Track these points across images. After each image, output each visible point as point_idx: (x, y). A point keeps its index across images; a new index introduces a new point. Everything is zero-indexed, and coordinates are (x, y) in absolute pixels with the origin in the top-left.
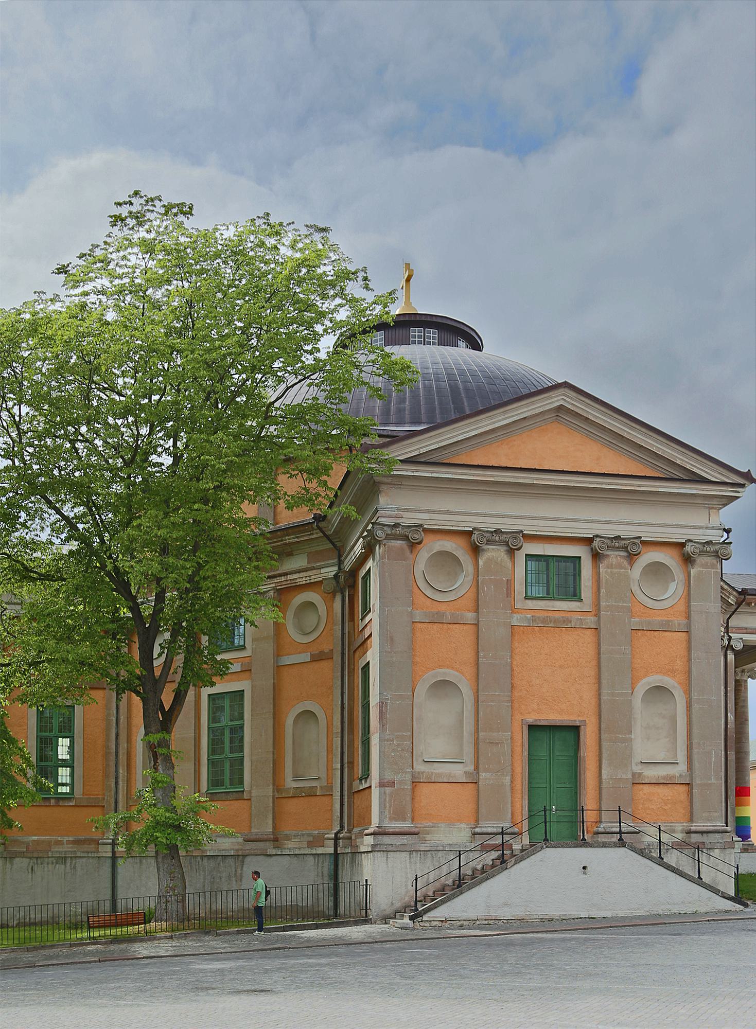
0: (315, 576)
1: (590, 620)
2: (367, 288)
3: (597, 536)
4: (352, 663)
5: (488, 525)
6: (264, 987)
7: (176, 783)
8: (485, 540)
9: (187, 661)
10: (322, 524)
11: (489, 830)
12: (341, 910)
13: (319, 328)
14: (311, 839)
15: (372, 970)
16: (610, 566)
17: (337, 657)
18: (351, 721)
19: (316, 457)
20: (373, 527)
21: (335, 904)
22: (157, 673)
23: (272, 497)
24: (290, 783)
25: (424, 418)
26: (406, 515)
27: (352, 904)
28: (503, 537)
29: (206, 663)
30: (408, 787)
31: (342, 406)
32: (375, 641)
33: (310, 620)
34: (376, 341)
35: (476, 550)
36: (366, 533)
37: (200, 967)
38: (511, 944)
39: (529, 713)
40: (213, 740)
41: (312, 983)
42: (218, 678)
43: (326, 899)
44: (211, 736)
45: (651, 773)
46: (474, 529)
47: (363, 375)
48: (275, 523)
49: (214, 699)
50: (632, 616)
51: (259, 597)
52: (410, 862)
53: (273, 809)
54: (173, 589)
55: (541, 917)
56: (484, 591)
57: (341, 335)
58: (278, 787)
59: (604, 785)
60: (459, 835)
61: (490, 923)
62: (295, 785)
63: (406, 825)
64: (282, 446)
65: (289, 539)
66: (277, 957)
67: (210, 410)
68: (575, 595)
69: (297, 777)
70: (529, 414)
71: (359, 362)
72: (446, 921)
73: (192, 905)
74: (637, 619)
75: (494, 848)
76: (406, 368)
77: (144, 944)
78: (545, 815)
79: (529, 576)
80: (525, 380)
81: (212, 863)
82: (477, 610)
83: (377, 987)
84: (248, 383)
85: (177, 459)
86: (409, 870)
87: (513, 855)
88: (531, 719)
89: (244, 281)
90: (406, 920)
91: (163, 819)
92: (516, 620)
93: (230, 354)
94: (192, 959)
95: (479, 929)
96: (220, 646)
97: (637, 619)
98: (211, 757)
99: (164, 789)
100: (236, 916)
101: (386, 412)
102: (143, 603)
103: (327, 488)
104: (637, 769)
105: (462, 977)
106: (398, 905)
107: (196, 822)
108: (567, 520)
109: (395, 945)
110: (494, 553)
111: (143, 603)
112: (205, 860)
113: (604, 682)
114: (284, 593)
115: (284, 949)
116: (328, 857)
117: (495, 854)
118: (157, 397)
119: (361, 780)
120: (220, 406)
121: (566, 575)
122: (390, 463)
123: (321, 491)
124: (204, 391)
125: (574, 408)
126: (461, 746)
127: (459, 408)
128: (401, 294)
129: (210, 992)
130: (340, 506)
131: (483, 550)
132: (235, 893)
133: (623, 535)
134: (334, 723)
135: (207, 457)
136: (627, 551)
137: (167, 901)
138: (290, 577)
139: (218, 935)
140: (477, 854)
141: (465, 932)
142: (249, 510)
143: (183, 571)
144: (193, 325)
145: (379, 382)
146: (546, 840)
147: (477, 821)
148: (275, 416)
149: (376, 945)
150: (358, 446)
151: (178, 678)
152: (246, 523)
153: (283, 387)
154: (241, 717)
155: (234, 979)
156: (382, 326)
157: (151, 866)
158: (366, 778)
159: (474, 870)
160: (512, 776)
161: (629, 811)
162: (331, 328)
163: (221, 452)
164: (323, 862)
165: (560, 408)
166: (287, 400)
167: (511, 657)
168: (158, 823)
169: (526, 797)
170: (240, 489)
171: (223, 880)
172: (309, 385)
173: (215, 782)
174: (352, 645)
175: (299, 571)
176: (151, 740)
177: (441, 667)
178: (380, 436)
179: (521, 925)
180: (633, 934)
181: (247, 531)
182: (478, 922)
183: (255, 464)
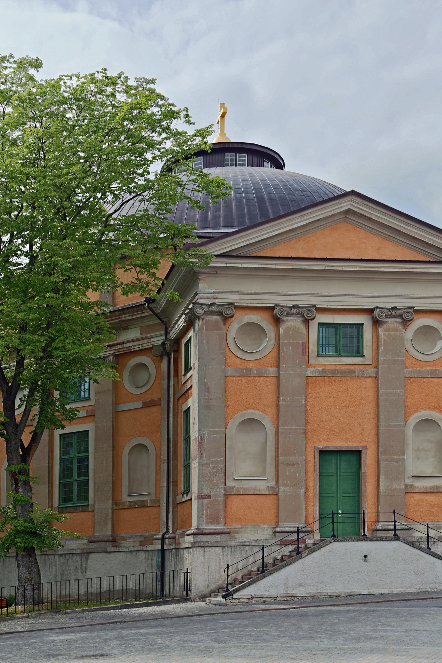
0: (146, 345)
1: (371, 371)
2: (189, 122)
3: (377, 307)
4: (176, 408)
5: (287, 302)
6: (103, 652)
7: (34, 500)
8: (285, 313)
9: (42, 411)
10: (152, 305)
11: (287, 529)
12: (167, 592)
13: (149, 156)
14: (142, 539)
15: (191, 637)
16: (388, 330)
17: (164, 404)
18: (175, 451)
19: (146, 255)
20: (193, 306)
21: (161, 589)
22: (18, 420)
23: (111, 286)
24: (126, 498)
25: (235, 222)
26: (220, 296)
27: (176, 587)
28: (300, 311)
29: (58, 411)
30: (222, 498)
31: (168, 216)
32: (195, 391)
33: (143, 376)
34: (196, 165)
35: (277, 321)
36: (187, 311)
37: (52, 638)
38: (305, 615)
39: (320, 441)
40: (63, 468)
41: (143, 648)
42: (68, 422)
43: (154, 583)
44: (62, 465)
45: (420, 484)
46: (276, 305)
47: (185, 191)
48: (114, 305)
49: (64, 438)
50: (406, 367)
51: (101, 361)
52: (223, 555)
53: (112, 517)
54: (30, 358)
55: (330, 594)
56: (284, 352)
57: (167, 161)
58: (116, 502)
59: (382, 494)
60: (263, 534)
61: (288, 599)
62: (129, 499)
63: (220, 527)
64: (119, 248)
65: (126, 317)
66: (114, 629)
67: (59, 220)
68: (358, 352)
69: (131, 494)
70: (322, 216)
71: (182, 181)
72: (252, 598)
73: (45, 591)
74: (410, 369)
75: (291, 543)
76: (220, 185)
77: (7, 624)
78: (333, 517)
79: (321, 339)
80: (320, 191)
81: (62, 560)
82: (278, 366)
83: (195, 650)
84: (91, 199)
85: (33, 259)
86: (222, 561)
87: (306, 548)
88: (321, 446)
89: (86, 122)
90: (219, 599)
91: (22, 528)
92: (309, 372)
93: (75, 179)
94: (45, 633)
95: (279, 604)
96: (69, 398)
97: (410, 369)
98: (62, 481)
99: (24, 506)
100: (81, 599)
101: (204, 218)
102: (6, 368)
103: (156, 278)
104: (408, 481)
105: (265, 641)
106: (213, 587)
107: (50, 529)
108: (353, 296)
109: (210, 617)
110: (292, 323)
111: (6, 368)
112: (57, 557)
113: (382, 417)
114: (121, 358)
115: (121, 622)
116: (156, 552)
117: (291, 548)
118: (16, 213)
119: (183, 494)
120: (68, 219)
121: (352, 337)
122: (207, 257)
123: (151, 280)
124: (55, 207)
125: (359, 210)
126: (265, 468)
127: (264, 213)
128: (217, 128)
129: (60, 658)
130: (166, 292)
131: (283, 321)
132: (81, 582)
133: (399, 306)
134: (162, 453)
135: (57, 258)
136: (402, 318)
137: (25, 590)
138: (126, 345)
139: (66, 613)
140: (277, 548)
141: (267, 606)
142: (92, 296)
143: (38, 344)
144: (45, 156)
145: (199, 196)
146: (333, 536)
147: (277, 523)
148: (114, 225)
149: (195, 618)
150: (181, 245)
151: (35, 423)
152: (90, 306)
153: (119, 202)
154: (87, 450)
155: (79, 647)
156: (201, 153)
157: (12, 563)
158: (187, 493)
159: (275, 560)
160: (306, 490)
161: (403, 513)
162: (158, 156)
163: (69, 253)
164: (152, 557)
165: (348, 211)
166: (124, 212)
167: (306, 400)
168: (18, 531)
169: (317, 504)
170: (85, 280)
171: (71, 572)
172: (141, 201)
173: (66, 498)
174: (176, 394)
175: (133, 341)
176: (13, 470)
177: (248, 409)
178: (199, 237)
179: (314, 600)
180: (405, 606)
181: (91, 312)
182: (278, 599)
183: (96, 261)
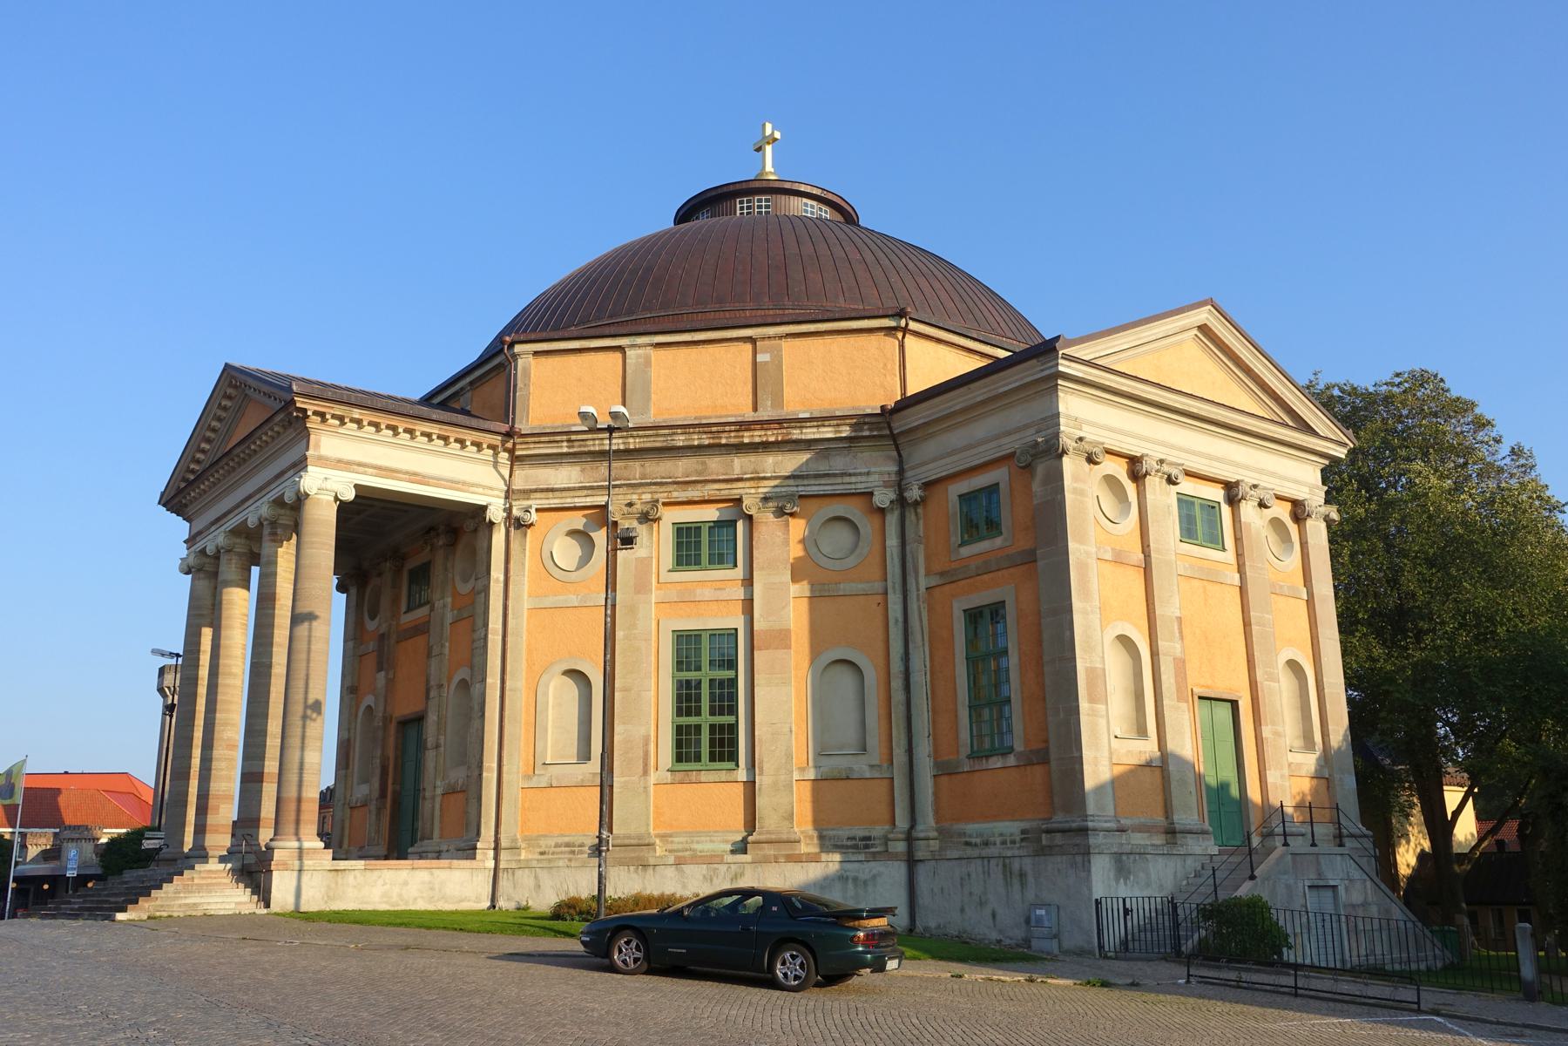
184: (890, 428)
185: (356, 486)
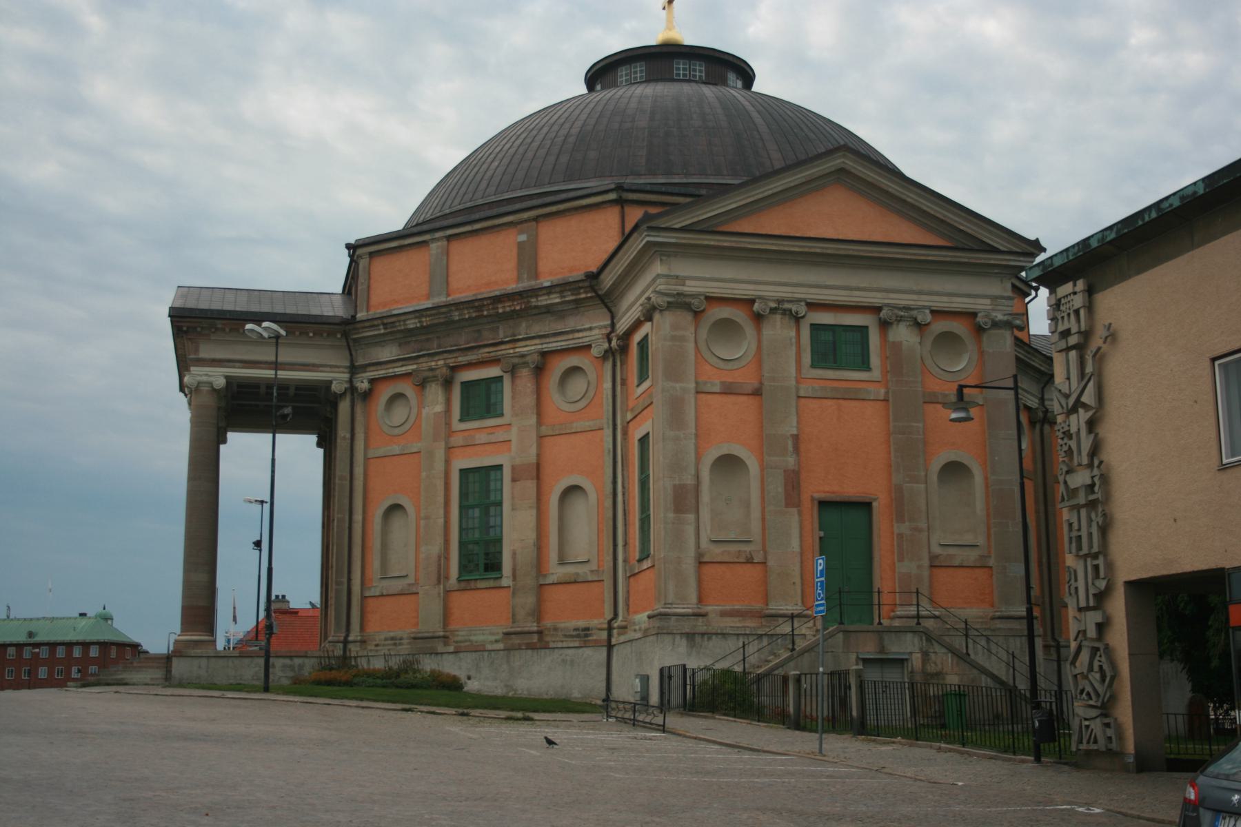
33: (577, 386)
69: (562, 562)
184: (595, 292)
185: (227, 377)
